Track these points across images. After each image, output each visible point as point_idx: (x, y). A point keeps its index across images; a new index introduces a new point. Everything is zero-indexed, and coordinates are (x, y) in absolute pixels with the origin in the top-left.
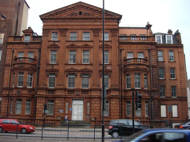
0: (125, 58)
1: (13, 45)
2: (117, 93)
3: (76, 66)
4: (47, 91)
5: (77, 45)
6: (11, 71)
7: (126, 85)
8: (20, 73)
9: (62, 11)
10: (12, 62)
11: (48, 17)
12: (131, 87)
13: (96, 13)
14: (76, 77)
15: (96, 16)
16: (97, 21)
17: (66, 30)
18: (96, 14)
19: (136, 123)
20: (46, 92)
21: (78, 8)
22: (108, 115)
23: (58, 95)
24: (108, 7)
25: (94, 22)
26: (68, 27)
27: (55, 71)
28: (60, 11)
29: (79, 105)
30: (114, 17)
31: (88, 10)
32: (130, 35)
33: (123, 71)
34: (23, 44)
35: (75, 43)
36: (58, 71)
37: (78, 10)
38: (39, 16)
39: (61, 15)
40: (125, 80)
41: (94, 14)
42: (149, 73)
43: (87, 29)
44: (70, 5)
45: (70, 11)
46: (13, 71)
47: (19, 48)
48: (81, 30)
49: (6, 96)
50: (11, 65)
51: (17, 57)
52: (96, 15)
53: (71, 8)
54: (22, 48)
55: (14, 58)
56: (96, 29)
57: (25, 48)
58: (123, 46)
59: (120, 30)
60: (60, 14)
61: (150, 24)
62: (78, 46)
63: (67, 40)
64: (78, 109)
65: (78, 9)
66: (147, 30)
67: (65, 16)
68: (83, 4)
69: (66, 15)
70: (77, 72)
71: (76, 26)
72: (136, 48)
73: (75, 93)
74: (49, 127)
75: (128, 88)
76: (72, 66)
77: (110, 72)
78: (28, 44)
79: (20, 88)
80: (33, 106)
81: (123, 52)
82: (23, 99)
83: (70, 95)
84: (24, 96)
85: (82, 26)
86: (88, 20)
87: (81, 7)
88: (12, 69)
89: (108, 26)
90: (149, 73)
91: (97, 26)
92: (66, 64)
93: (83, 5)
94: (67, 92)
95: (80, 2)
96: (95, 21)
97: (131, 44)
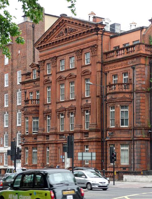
3: (65, 103)
4: (45, 136)
7: (110, 121)
8: (122, 107)
9: (53, 30)
14: (65, 117)
15: (80, 30)
20: (44, 138)
21: (63, 24)
24: (83, 15)
25: (76, 40)
26: (57, 55)
27: (63, 111)
28: (48, 34)
30: (90, 29)
31: (56, 32)
36: (75, 109)
39: (50, 40)
43: (64, 55)
44: (52, 26)
45: (57, 31)
47: (29, 87)
51: (111, 84)
53: (56, 27)
54: (32, 87)
58: (108, 66)
60: (50, 37)
63: (58, 71)
65: (64, 25)
67: (54, 39)
70: (65, 110)
72: (120, 67)
75: (62, 130)
78: (35, 81)
79: (124, 128)
80: (30, 155)
82: (29, 147)
84: (29, 144)
90: (132, 102)
94: (58, 137)
96: (77, 39)
97: (115, 62)
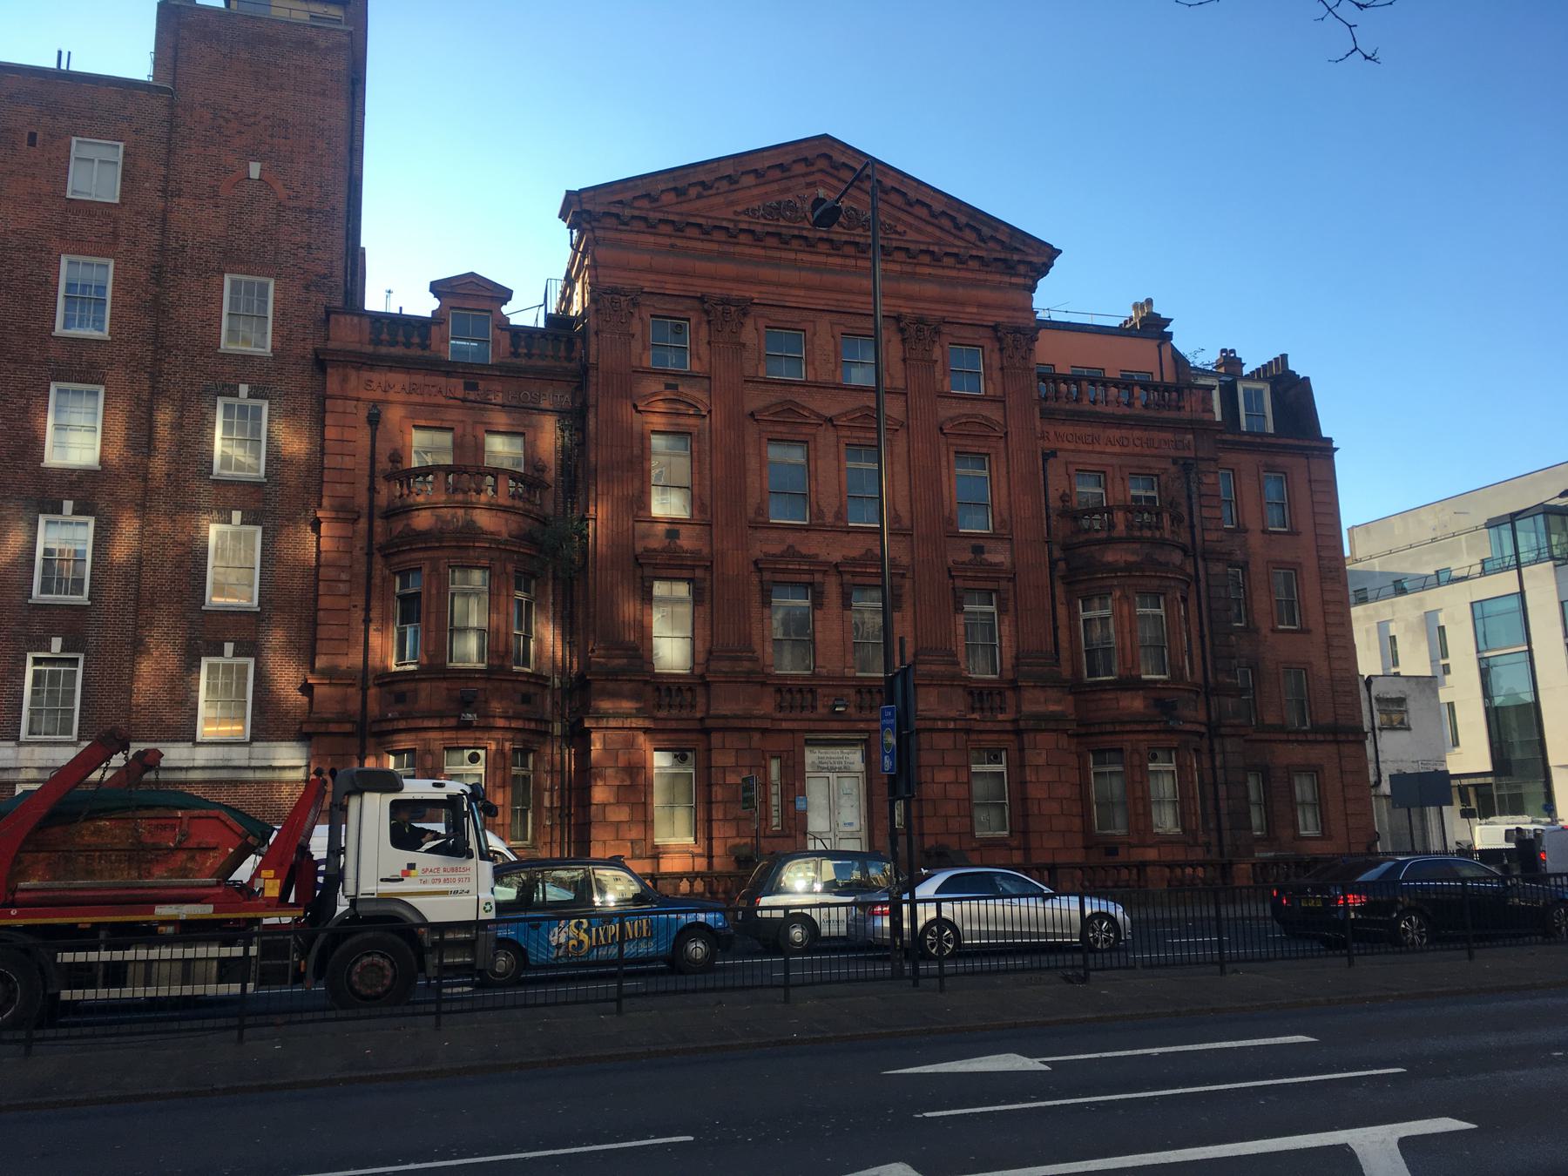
0: (1064, 498)
1: (366, 375)
2: (1054, 704)
5: (812, 412)
6: (370, 554)
10: (372, 489)
11: (627, 212)
12: (1115, 669)
13: (910, 220)
16: (919, 270)
17: (745, 307)
18: (911, 225)
19: (879, 909)
22: (1006, 833)
23: (725, 717)
26: (753, 293)
29: (844, 770)
32: (1069, 371)
33: (1063, 578)
34: (448, 374)
35: (800, 397)
37: (809, 185)
38: (1060, 252)
40: (1072, 629)
41: (900, 228)
42: (1193, 587)
46: (385, 556)
48: (828, 317)
49: (348, 728)
50: (365, 511)
52: (912, 235)
55: (383, 464)
56: (726, 302)
57: (464, 400)
59: (1045, 339)
61: (1155, 310)
62: (819, 416)
64: (832, 810)
66: (1159, 346)
68: (843, 153)
69: (736, 213)
71: (802, 293)
73: (819, 704)
74: (169, 998)
76: (791, 538)
77: (1009, 580)
81: (1056, 469)
83: (792, 715)
85: (840, 297)
86: (796, 251)
87: (821, 171)
88: (379, 539)
89: (982, 310)
91: (921, 305)
92: (755, 526)
93: (839, 158)
95: (826, 136)
